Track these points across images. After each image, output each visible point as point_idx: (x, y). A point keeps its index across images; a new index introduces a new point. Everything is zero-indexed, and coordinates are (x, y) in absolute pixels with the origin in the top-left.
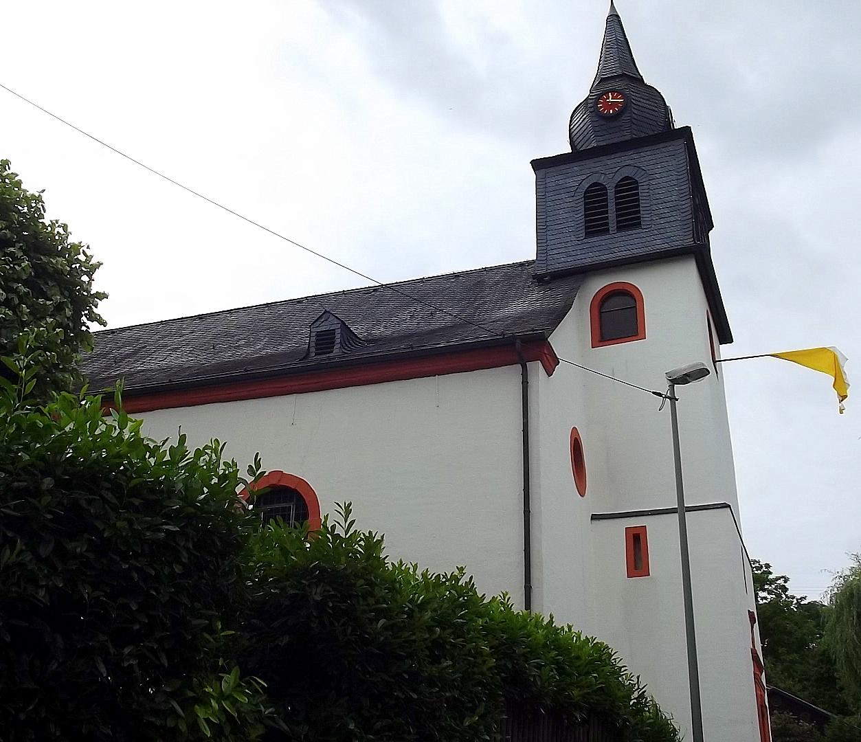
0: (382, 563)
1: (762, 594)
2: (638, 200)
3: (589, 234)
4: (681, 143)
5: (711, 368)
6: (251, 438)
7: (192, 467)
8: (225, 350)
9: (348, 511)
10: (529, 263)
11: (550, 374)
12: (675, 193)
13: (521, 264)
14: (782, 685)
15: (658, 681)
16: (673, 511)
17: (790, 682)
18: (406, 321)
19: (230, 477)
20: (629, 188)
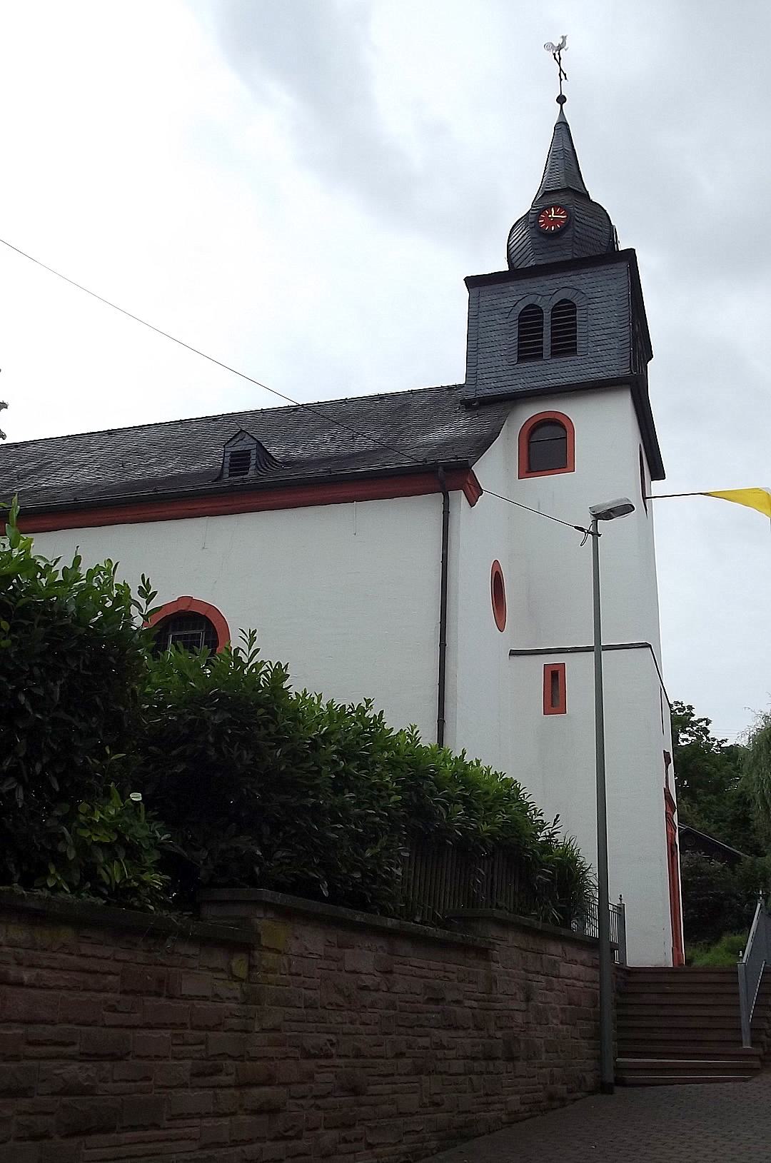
0: (285, 692)
1: (682, 736)
3: (521, 359)
4: (624, 266)
5: (636, 501)
6: (159, 564)
7: (86, 591)
9: (252, 638)
10: (461, 386)
11: (472, 505)
13: (449, 388)
14: (698, 825)
15: (561, 811)
17: (706, 822)
18: (327, 444)
19: (123, 598)
20: (566, 310)
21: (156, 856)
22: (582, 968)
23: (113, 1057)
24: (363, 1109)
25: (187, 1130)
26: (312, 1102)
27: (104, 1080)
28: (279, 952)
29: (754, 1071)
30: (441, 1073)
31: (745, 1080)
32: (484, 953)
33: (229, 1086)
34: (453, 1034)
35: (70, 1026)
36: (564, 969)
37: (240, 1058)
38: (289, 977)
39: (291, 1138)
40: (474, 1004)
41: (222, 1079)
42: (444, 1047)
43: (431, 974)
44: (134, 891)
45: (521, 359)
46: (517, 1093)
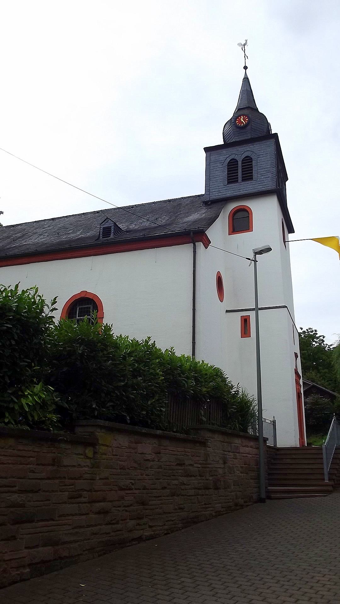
0: (112, 336)
2: (252, 167)
3: (229, 183)
4: (273, 141)
6: (52, 285)
7: (20, 298)
8: (63, 235)
10: (202, 195)
12: (269, 164)
14: (319, 383)
16: (253, 310)
20: (248, 161)
21: (54, 407)
22: (251, 449)
23: (32, 491)
24: (147, 511)
25: (66, 521)
26: (123, 509)
27: (29, 501)
28: (108, 446)
29: (330, 492)
30: (183, 495)
31: (325, 496)
32: (204, 444)
33: (85, 503)
34: (189, 478)
35: (14, 479)
36: (242, 450)
37: (90, 491)
38: (112, 457)
39: (113, 524)
40: (199, 466)
41: (83, 499)
42: (184, 484)
43: (179, 453)
44: (43, 422)
45: (229, 183)
46: (219, 503)
